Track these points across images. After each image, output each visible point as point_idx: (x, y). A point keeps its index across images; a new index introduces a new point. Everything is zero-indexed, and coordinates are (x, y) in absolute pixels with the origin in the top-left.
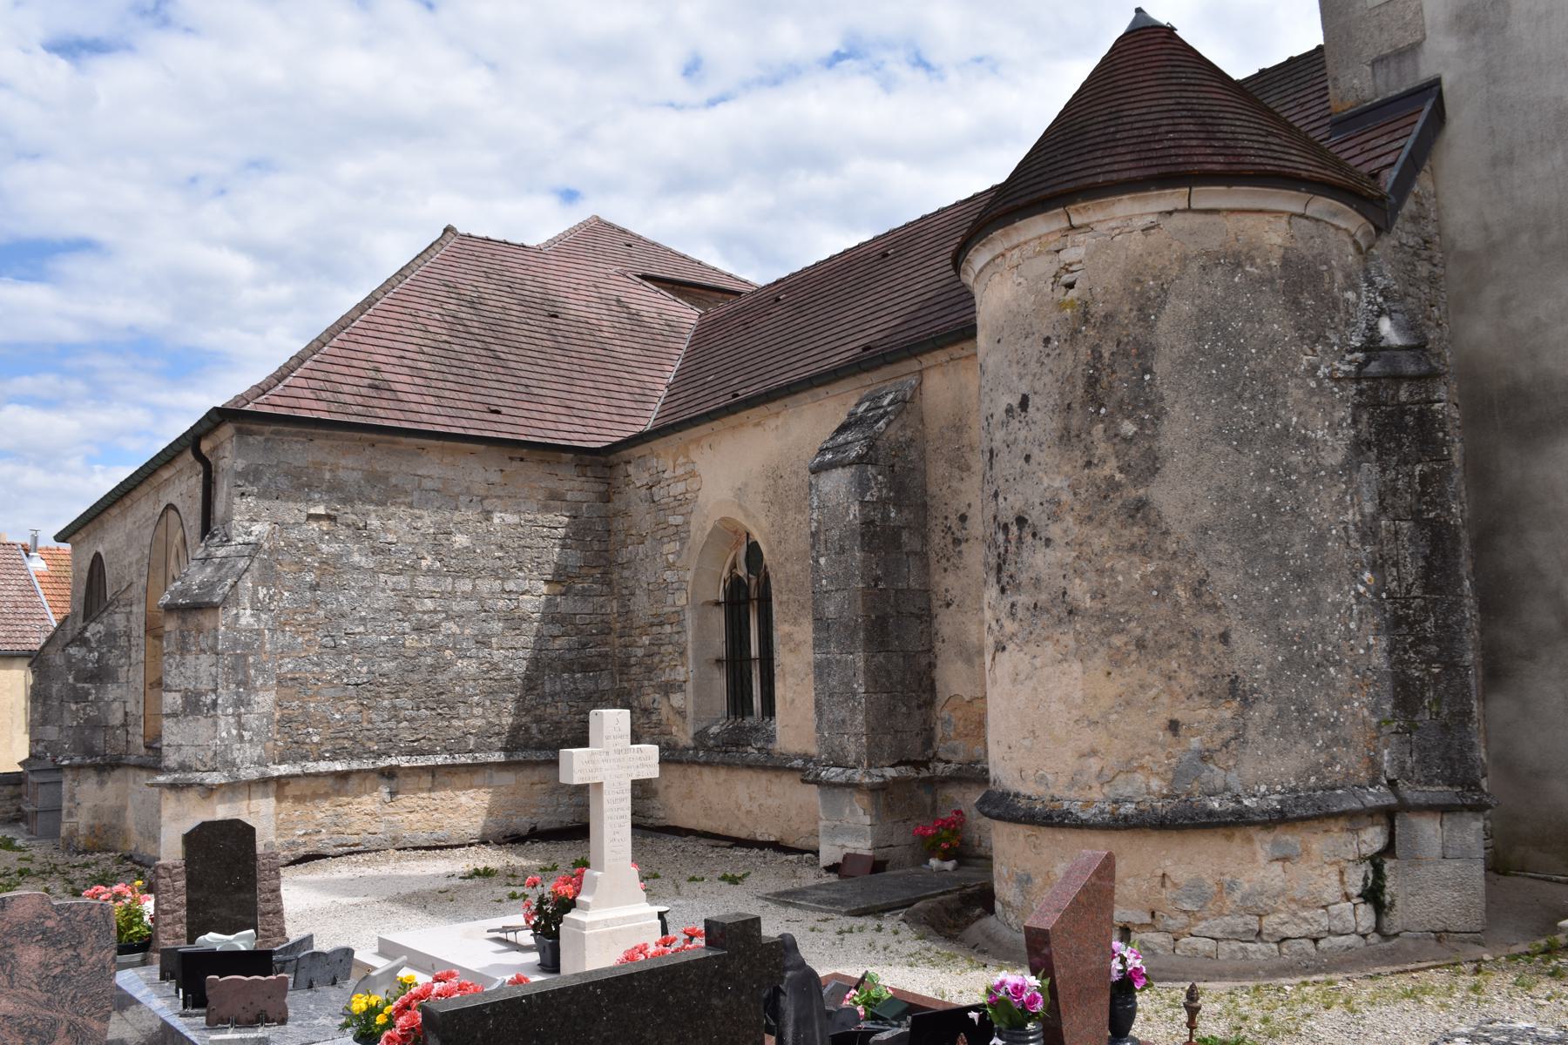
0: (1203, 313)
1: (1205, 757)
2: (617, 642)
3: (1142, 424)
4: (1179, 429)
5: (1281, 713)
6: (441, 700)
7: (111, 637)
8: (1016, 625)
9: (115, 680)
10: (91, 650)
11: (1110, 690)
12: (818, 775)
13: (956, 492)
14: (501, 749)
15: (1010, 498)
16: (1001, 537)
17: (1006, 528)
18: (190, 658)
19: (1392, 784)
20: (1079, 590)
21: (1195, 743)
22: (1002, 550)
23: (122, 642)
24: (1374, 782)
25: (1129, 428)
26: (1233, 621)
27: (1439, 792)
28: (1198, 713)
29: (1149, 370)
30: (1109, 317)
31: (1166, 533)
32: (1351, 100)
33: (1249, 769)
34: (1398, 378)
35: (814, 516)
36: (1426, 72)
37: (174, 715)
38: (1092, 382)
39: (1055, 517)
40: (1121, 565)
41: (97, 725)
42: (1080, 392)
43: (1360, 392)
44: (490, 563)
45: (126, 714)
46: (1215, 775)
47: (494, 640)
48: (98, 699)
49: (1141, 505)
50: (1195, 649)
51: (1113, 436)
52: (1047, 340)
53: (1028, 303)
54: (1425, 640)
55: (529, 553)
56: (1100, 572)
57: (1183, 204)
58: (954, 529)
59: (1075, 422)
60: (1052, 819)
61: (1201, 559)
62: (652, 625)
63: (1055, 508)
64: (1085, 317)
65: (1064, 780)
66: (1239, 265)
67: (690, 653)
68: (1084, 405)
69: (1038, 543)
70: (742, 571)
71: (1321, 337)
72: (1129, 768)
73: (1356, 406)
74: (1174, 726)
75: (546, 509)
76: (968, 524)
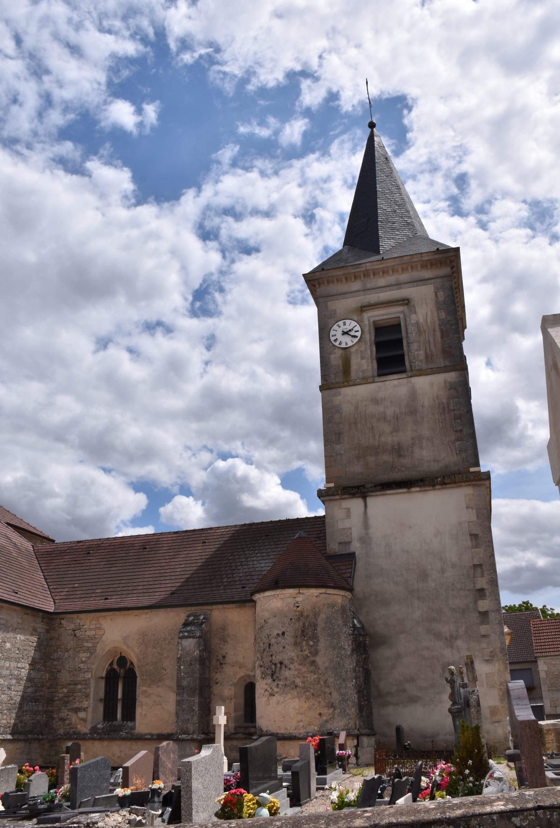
1: (326, 721)
2: (47, 690)
3: (314, 642)
4: (322, 644)
5: (341, 711)
8: (279, 690)
12: (178, 737)
14: (10, 734)
15: (277, 657)
16: (273, 667)
17: (275, 664)
19: (358, 730)
20: (298, 681)
21: (324, 718)
22: (274, 670)
24: (356, 728)
25: (311, 643)
27: (366, 731)
28: (325, 711)
29: (316, 630)
30: (308, 616)
31: (319, 669)
34: (360, 635)
35: (180, 652)
36: (352, 549)
38: (303, 631)
39: (292, 663)
40: (309, 675)
42: (300, 633)
43: (353, 638)
44: (13, 655)
47: (13, 687)
50: (325, 696)
51: (308, 645)
52: (291, 619)
54: (364, 696)
56: (304, 677)
57: (324, 592)
58: (220, 660)
60: (291, 738)
61: (326, 675)
62: (70, 684)
63: (292, 661)
64: (302, 615)
65: (293, 728)
66: (334, 607)
67: (91, 696)
68: (301, 637)
69: (286, 669)
70: (115, 666)
71: (346, 625)
72: (310, 724)
73: (352, 641)
74: (320, 714)
75: (32, 635)
76: (226, 659)
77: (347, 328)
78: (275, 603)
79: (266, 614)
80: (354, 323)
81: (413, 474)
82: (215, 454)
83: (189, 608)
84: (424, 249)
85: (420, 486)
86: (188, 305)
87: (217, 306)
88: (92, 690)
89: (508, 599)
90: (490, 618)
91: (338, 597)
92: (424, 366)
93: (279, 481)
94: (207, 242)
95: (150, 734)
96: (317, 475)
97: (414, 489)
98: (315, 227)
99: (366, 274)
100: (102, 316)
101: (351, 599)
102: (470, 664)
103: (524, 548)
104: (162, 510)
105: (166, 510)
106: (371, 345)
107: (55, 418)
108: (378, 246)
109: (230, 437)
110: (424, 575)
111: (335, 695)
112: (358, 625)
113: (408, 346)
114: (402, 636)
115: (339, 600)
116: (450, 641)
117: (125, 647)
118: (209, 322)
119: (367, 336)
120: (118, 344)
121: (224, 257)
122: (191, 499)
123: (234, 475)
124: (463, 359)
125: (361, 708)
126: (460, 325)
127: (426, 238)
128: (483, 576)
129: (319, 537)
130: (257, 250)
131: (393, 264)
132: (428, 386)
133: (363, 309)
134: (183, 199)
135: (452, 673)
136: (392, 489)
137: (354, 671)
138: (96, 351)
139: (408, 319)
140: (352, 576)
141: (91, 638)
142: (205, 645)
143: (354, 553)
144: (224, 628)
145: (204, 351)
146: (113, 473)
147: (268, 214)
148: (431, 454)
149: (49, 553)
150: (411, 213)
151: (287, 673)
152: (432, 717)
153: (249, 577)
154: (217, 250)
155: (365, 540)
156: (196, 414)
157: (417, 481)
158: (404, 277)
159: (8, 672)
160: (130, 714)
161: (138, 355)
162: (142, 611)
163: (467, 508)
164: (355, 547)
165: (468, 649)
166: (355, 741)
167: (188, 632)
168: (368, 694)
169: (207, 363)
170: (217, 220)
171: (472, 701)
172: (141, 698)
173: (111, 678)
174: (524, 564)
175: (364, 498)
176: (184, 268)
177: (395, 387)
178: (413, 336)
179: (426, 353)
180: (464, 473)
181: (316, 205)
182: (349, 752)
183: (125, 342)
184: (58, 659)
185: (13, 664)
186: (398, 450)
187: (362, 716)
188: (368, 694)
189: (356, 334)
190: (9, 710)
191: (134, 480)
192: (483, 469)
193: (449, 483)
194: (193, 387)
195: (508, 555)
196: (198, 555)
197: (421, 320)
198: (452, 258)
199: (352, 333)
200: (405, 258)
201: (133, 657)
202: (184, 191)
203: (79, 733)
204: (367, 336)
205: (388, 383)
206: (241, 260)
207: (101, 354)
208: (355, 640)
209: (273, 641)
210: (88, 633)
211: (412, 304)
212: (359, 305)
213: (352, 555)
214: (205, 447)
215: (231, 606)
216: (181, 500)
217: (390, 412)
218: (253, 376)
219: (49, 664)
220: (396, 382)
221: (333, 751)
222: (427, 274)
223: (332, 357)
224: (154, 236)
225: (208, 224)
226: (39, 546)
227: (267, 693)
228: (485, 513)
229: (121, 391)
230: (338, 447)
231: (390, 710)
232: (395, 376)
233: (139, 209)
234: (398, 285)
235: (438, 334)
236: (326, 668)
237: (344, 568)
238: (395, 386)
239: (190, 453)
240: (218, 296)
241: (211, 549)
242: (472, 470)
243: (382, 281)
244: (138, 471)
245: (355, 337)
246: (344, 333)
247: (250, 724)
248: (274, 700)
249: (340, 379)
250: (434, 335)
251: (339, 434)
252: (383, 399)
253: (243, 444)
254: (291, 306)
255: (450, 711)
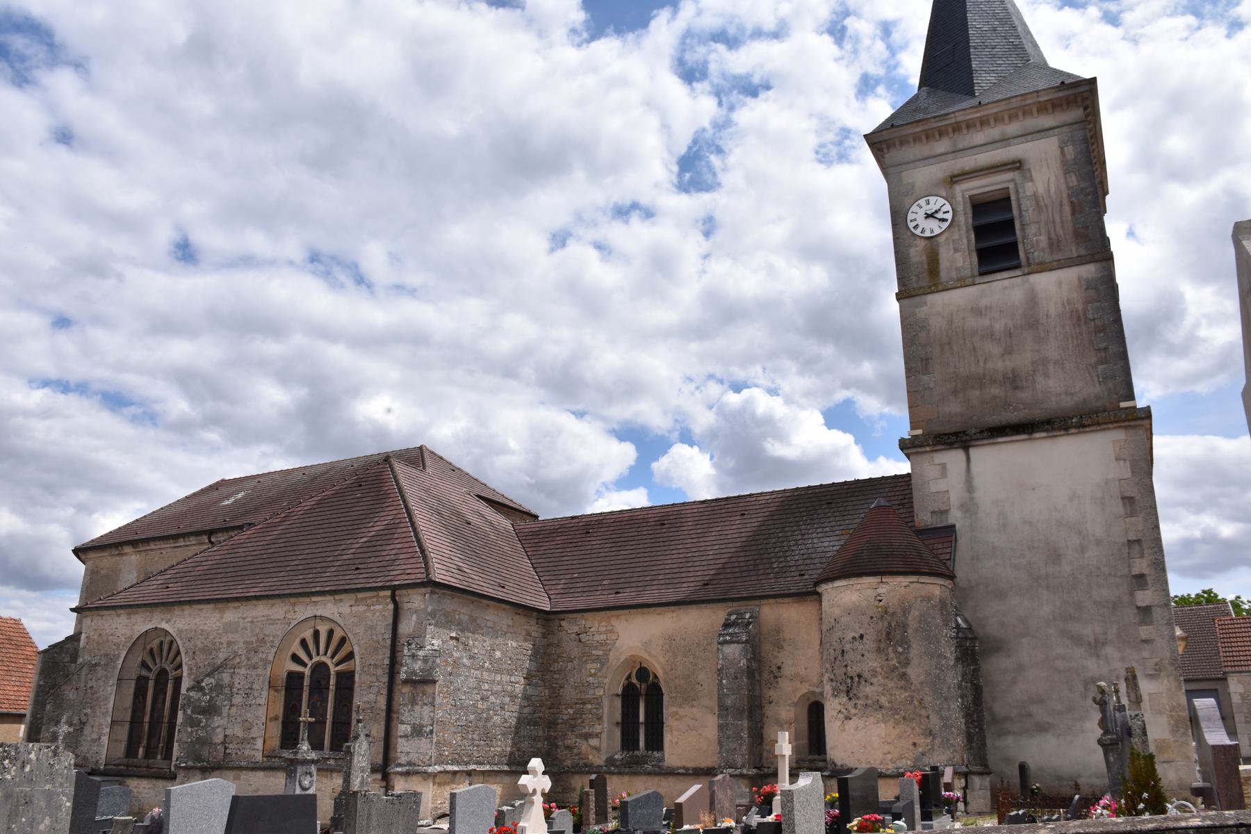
0: (921, 615)
4: (916, 650)
6: (488, 737)
7: (219, 687)
9: (220, 714)
10: (205, 694)
11: (895, 732)
13: (776, 657)
16: (849, 681)
18: (417, 708)
23: (227, 690)
25: (900, 650)
26: (930, 712)
30: (894, 613)
32: (923, 524)
33: (935, 758)
34: (966, 638)
36: (951, 521)
37: (406, 736)
38: (888, 634)
39: (874, 676)
41: (204, 742)
45: (226, 736)
46: (926, 760)
48: (207, 726)
49: (904, 674)
51: (895, 651)
53: (864, 604)
55: (520, 663)
59: (882, 645)
67: (605, 718)
70: (634, 681)
74: (914, 744)
75: (525, 640)
77: (931, 208)
78: (846, 596)
79: (837, 611)
80: (941, 201)
81: (1036, 413)
82: (726, 385)
83: (730, 604)
84: (1042, 85)
85: (1046, 431)
86: (674, 179)
87: (714, 174)
88: (606, 710)
89: (1180, 586)
90: (1155, 615)
91: (935, 588)
92: (1047, 258)
93: (823, 421)
94: (695, 84)
95: (684, 768)
96: (895, 417)
97: (1037, 435)
98: (848, 46)
99: (957, 128)
100: (552, 202)
101: (952, 590)
102: (1132, 680)
103: (1198, 508)
104: (655, 465)
105: (661, 465)
106: (967, 231)
107: (504, 346)
108: (972, 85)
109: (747, 360)
110: (1055, 556)
111: (935, 720)
112: (963, 625)
113: (1023, 230)
114: (1024, 640)
115: (937, 591)
116: (1095, 647)
117: (646, 656)
118: (705, 197)
119: (961, 219)
120: (579, 239)
121: (720, 104)
122: (696, 448)
123: (753, 415)
124: (1105, 242)
125: (970, 738)
126: (1100, 193)
127: (1044, 65)
128: (1142, 557)
129: (903, 505)
130: (768, 87)
131: (995, 110)
132: (1055, 287)
133: (954, 179)
134: (653, 24)
135: (1102, 691)
136: (1007, 435)
137: (960, 687)
138: (552, 250)
139: (1021, 190)
140: (952, 558)
141: (602, 644)
142: (754, 653)
143: (954, 526)
144: (778, 631)
145: (701, 238)
146: (587, 417)
147: (778, 34)
148: (1062, 385)
149: (535, 534)
150: (1019, 29)
151: (868, 689)
152: (1077, 751)
153: (808, 561)
154: (710, 93)
155: (969, 507)
156: (696, 331)
157: (1043, 422)
158: (1013, 128)
159: (499, 688)
160: (656, 741)
161: (610, 253)
162: (666, 608)
163: (1117, 459)
164: (956, 517)
165: (1122, 659)
166: (963, 781)
167: (730, 635)
168: (979, 720)
169: (706, 257)
170: (701, 50)
171: (1136, 730)
172: (669, 722)
173: (629, 696)
174: (1197, 534)
175: (966, 448)
176: (665, 126)
177: (1005, 290)
178: (1029, 212)
179: (1050, 239)
180: (1115, 412)
181: (847, 13)
182: (959, 794)
183: (592, 235)
184: (559, 672)
185: (506, 678)
186: (1013, 380)
187: (971, 748)
188: (979, 720)
189: (945, 216)
190: (503, 734)
191: (616, 427)
192: (1140, 403)
193: (1089, 426)
194: (687, 295)
195: (1174, 520)
196: (736, 531)
197: (1041, 190)
198: (1085, 95)
199: (940, 215)
200: (1013, 100)
201: (658, 666)
202: (655, 12)
203: (591, 765)
204: (961, 219)
205: (994, 284)
206: (744, 104)
207: (559, 253)
208: (959, 646)
209: (847, 647)
210: (597, 638)
211: (1026, 167)
212: (948, 174)
213: (951, 529)
214: (711, 377)
215: (786, 600)
216: (681, 451)
217: (999, 326)
218: (770, 269)
219: (548, 677)
220: (1006, 283)
221: (939, 792)
222: (1047, 121)
223: (913, 251)
224: (621, 82)
225: (690, 58)
226: (521, 524)
227: (841, 716)
228: (1144, 463)
229: (590, 305)
230: (925, 378)
231: (1009, 741)
232: (1005, 274)
233: (596, 45)
234: (1005, 141)
235: (1067, 209)
236: (922, 683)
237: (940, 546)
238: (1005, 288)
239: (693, 386)
240: (714, 159)
241: (753, 522)
242: (1123, 405)
243: (979, 137)
244: (621, 412)
245: (944, 220)
246: (928, 216)
247: (816, 757)
248: (851, 725)
249: (924, 282)
250: (1061, 211)
251: (927, 361)
252: (989, 308)
253: (764, 369)
254: (822, 166)
255: (1100, 742)
